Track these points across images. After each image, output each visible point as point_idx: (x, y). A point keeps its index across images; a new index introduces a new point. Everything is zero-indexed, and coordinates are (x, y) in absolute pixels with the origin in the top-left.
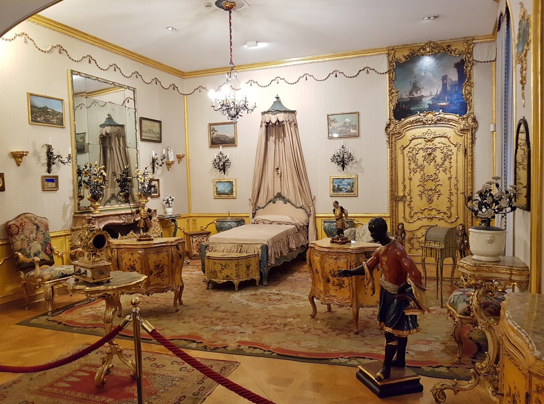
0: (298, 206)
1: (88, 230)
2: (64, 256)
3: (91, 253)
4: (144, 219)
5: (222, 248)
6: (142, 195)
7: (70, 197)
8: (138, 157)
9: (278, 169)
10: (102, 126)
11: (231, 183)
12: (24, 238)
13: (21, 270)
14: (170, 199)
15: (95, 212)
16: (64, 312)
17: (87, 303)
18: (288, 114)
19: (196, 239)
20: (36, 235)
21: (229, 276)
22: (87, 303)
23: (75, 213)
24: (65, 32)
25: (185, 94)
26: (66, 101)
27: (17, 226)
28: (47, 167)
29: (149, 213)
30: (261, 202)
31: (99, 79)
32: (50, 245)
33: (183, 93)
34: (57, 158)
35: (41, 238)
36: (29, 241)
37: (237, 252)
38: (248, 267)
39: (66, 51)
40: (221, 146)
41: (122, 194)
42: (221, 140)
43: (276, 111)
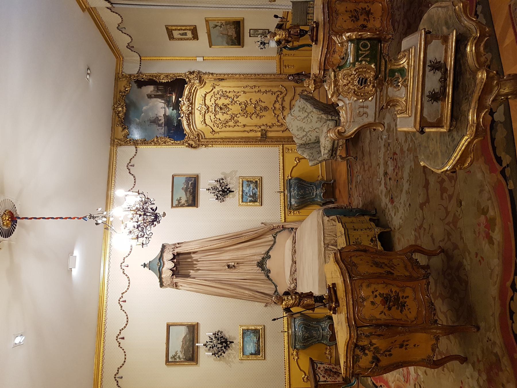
0: (272, 243)
9: (229, 266)
11: (245, 332)
19: (321, 376)
40: (197, 344)
42: (188, 347)
43: (160, 261)
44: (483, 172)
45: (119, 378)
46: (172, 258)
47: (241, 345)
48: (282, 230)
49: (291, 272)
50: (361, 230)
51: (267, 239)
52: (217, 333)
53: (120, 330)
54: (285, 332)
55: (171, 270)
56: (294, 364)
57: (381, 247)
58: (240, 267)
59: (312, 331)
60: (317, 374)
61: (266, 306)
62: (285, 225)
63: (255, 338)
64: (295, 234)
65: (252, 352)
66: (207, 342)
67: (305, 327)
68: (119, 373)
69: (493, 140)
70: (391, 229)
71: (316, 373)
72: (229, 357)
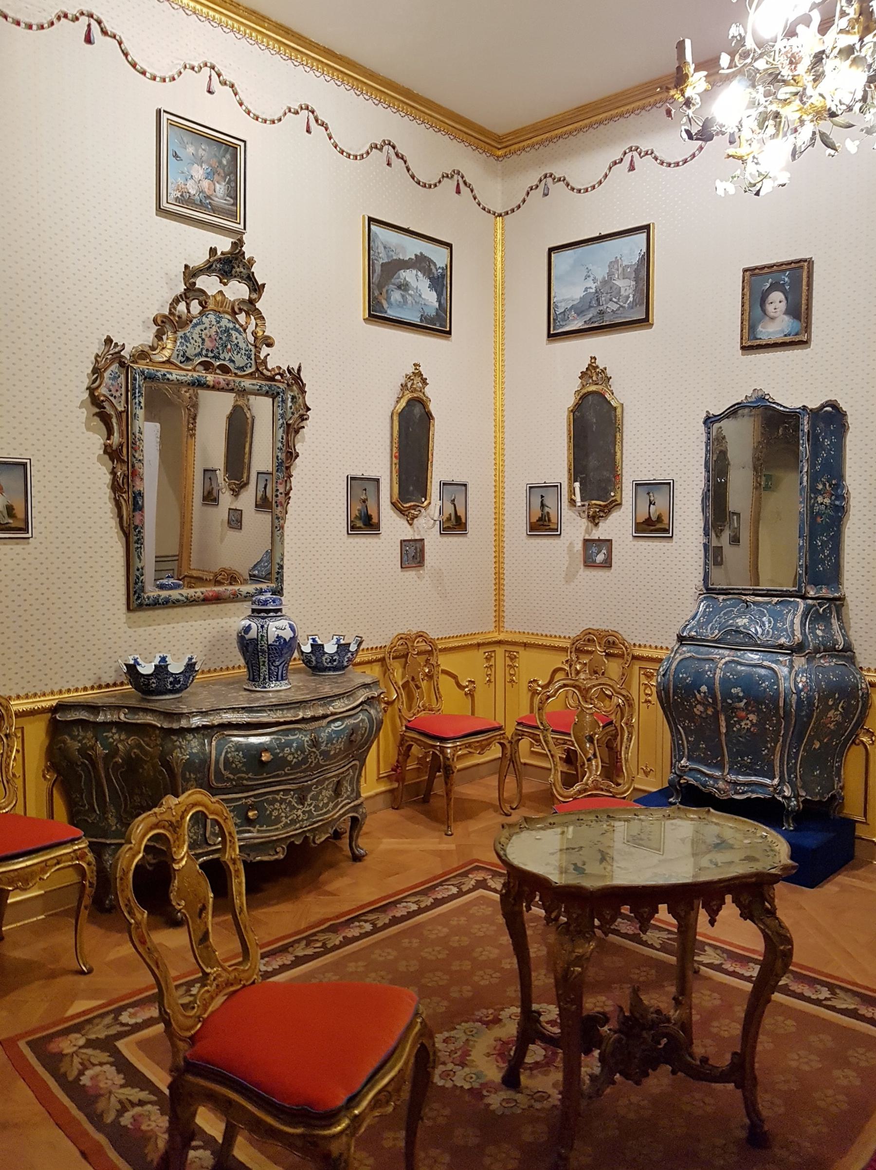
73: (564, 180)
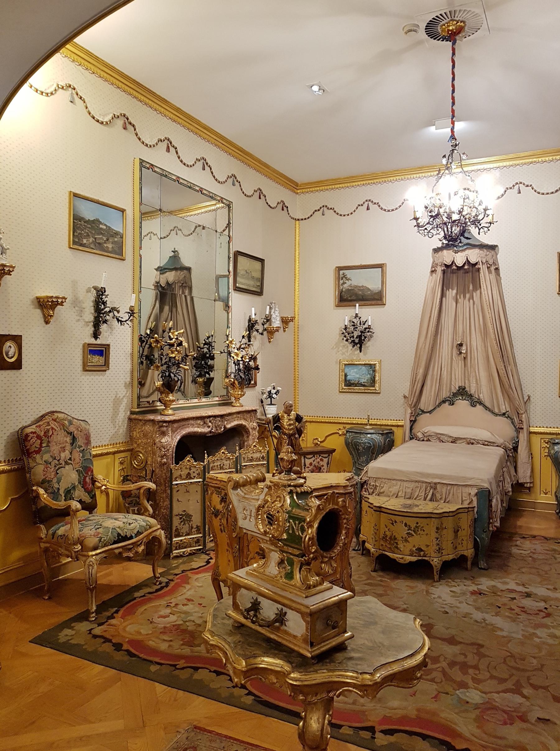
0: (496, 411)
1: (291, 493)
2: (111, 493)
3: (296, 559)
4: (290, 436)
5: (394, 489)
6: (236, 382)
7: (126, 383)
8: (230, 317)
9: (461, 345)
10: (162, 270)
11: (372, 367)
12: (51, 460)
13: (41, 522)
14: (273, 391)
15: (166, 412)
16: (120, 613)
17: (157, 591)
18: (485, 251)
19: (311, 460)
20: (71, 453)
21: (422, 550)
22: (157, 591)
23: (132, 413)
24: (135, 93)
25: (297, 218)
26: (129, 213)
27: (39, 437)
28: (93, 329)
29: (297, 423)
30: (426, 402)
31: (181, 181)
32: (92, 471)
33: (295, 217)
34: (110, 312)
35: (77, 460)
36: (59, 467)
37: (425, 499)
38: (456, 532)
39: (134, 126)
40: (357, 305)
41: (201, 380)
42: (356, 295)
43: (464, 245)
44: (395, 709)
45: (323, 211)
46: (471, 262)
47: (356, 363)
48: (515, 427)
49: (440, 434)
50: (437, 539)
51: (503, 403)
52: (371, 330)
53: (378, 203)
54: (368, 421)
55: (453, 261)
56: (333, 429)
57: (409, 561)
58: (460, 362)
59: (366, 456)
60: (314, 456)
61: (405, 397)
62: (523, 433)
63: (365, 381)
64: (497, 446)
65: (348, 376)
66: (359, 319)
67: (370, 447)
68: (328, 211)
69: (424, 737)
70: (437, 582)
71: (316, 456)
72: (344, 346)
73: (334, 209)
